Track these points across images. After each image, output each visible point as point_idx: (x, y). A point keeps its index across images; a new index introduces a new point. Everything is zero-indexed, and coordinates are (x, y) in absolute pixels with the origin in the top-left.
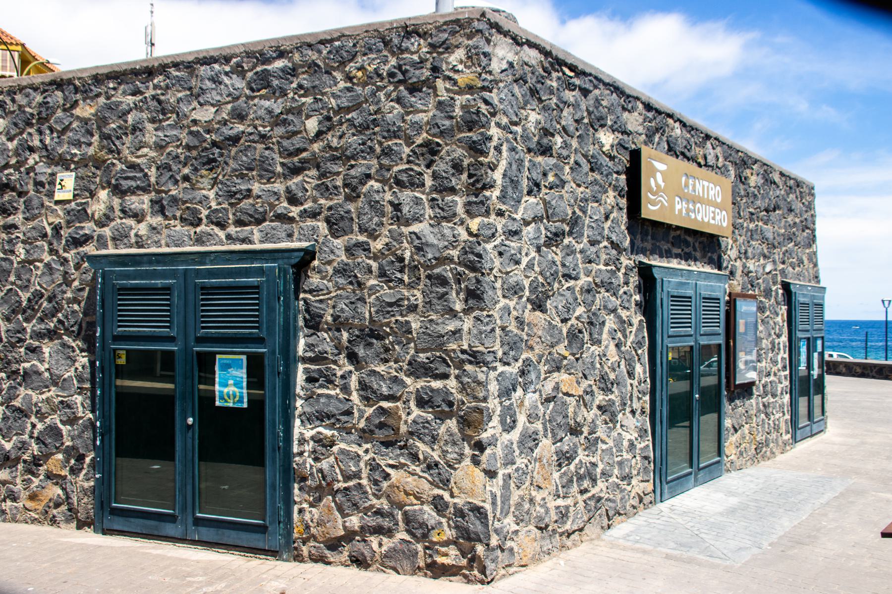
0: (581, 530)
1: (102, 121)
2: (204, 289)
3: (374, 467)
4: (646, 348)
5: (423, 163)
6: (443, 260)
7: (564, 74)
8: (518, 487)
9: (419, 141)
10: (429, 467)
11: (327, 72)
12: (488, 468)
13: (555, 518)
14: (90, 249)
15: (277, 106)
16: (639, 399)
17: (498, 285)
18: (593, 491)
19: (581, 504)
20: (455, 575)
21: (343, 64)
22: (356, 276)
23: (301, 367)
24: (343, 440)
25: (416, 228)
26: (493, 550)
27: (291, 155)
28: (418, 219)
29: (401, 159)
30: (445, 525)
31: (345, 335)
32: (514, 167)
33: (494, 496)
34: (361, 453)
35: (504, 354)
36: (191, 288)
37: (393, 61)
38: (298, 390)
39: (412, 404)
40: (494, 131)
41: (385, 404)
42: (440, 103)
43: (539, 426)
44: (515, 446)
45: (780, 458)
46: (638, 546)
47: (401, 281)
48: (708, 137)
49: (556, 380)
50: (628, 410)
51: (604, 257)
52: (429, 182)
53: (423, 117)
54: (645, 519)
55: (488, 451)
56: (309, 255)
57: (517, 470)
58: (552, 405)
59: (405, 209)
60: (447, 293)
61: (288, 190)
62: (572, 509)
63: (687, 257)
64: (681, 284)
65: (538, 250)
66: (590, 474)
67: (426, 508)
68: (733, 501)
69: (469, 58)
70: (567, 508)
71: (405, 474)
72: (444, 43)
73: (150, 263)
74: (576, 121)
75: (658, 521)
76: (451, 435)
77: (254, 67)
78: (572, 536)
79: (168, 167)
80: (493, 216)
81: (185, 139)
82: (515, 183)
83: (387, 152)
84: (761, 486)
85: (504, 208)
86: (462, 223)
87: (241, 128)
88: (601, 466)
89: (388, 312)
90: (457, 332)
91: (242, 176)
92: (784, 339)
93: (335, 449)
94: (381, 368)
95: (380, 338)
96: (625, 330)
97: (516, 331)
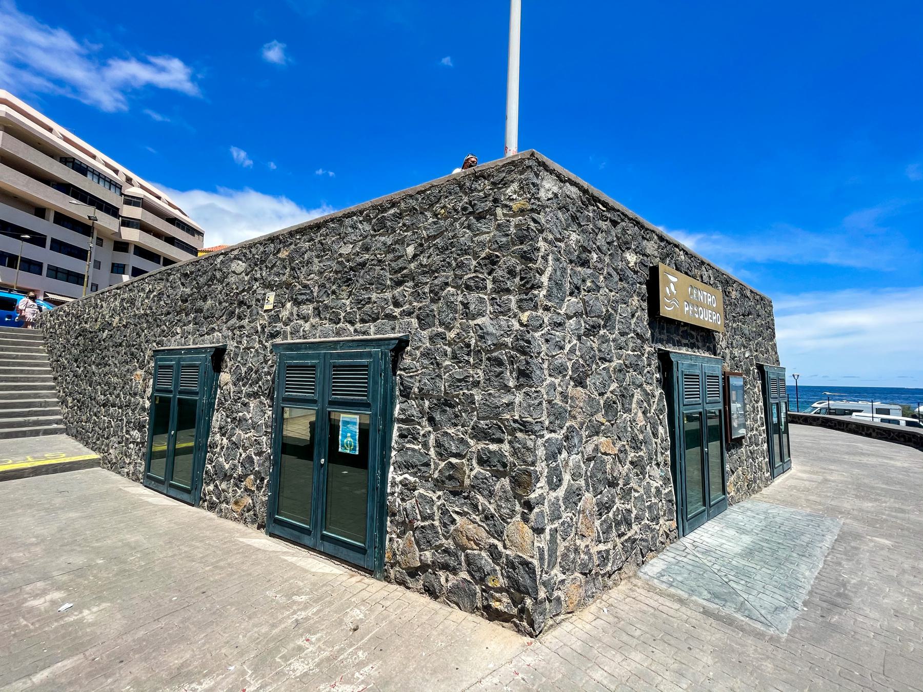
0: (620, 569)
1: (292, 259)
2: (336, 367)
3: (445, 512)
4: (666, 414)
5: (486, 271)
6: (499, 346)
7: (598, 208)
8: (564, 540)
9: (483, 255)
10: (487, 518)
11: (421, 213)
12: (536, 527)
13: (598, 563)
14: (278, 341)
15: (389, 240)
16: (662, 454)
17: (545, 366)
18: (629, 534)
19: (620, 546)
20: (506, 621)
21: (431, 205)
22: (435, 358)
23: (396, 426)
24: (422, 486)
25: (479, 321)
26: (541, 602)
27: (396, 272)
28: (481, 314)
29: (470, 270)
30: (499, 572)
31: (427, 403)
32: (558, 273)
33: (541, 551)
34: (434, 498)
35: (551, 423)
36: (328, 365)
37: (466, 199)
38: (393, 444)
39: (474, 462)
40: (541, 244)
41: (454, 460)
42: (499, 225)
43: (582, 482)
44: (561, 503)
45: (765, 491)
46: (672, 590)
47: (468, 362)
48: (703, 263)
49: (596, 443)
50: (654, 462)
51: (631, 345)
52: (490, 286)
53: (486, 237)
54: (673, 555)
55: (536, 510)
56: (402, 344)
57: (563, 524)
58: (592, 464)
59: (472, 307)
60: (502, 372)
61: (394, 297)
62: (611, 552)
63: (692, 346)
64: (691, 366)
65: (579, 338)
66: (626, 519)
67: (483, 554)
68: (747, 540)
69: (522, 188)
70: (607, 551)
71: (467, 521)
72: (502, 180)
73: (306, 349)
74: (608, 243)
75: (685, 560)
76: (505, 492)
77: (377, 216)
78: (613, 576)
79: (323, 286)
80: (541, 311)
81: (335, 267)
82: (559, 285)
83: (460, 265)
84: (764, 523)
85: (549, 304)
86: (515, 316)
87: (367, 256)
88: (635, 512)
89: (458, 386)
90: (510, 405)
91: (366, 289)
92: (761, 404)
93: (416, 493)
94: (451, 431)
95: (452, 406)
96: (649, 401)
97: (560, 403)
